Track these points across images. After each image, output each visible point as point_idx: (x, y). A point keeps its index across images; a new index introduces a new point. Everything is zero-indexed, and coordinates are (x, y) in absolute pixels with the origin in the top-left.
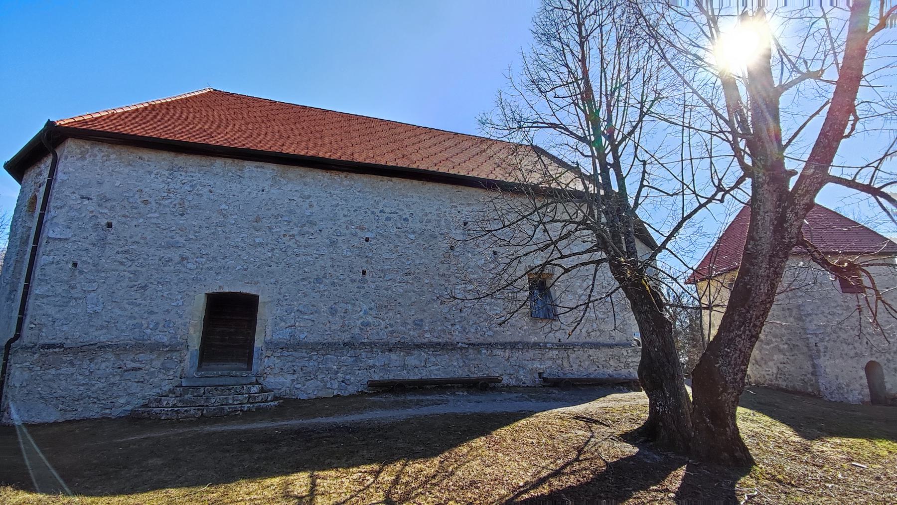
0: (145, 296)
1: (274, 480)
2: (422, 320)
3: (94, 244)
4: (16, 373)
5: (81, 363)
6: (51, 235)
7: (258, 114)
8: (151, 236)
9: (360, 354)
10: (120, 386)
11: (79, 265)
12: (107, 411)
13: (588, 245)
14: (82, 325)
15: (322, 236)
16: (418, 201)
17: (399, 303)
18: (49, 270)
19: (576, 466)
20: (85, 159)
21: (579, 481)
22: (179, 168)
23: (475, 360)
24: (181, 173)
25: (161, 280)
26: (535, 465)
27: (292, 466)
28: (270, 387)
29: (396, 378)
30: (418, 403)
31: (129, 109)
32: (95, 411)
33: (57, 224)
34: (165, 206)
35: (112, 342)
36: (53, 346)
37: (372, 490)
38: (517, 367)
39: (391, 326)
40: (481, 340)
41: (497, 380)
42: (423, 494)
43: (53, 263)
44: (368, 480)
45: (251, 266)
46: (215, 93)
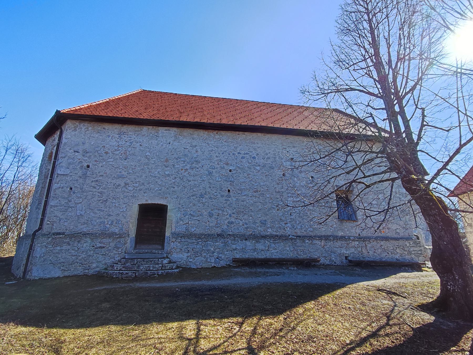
0: (106, 206)
1: (174, 324)
2: (265, 221)
3: (80, 177)
4: (38, 250)
5: (73, 243)
6: (59, 172)
7: (167, 101)
8: (109, 172)
9: (228, 242)
10: (93, 257)
11: (73, 189)
12: (87, 271)
13: (383, 169)
14: (74, 222)
15: (203, 169)
16: (261, 146)
17: (251, 210)
18: (58, 192)
19: (388, 330)
20: (76, 130)
21: (393, 342)
22: (124, 133)
23: (301, 246)
24: (125, 135)
25: (114, 197)
26: (355, 326)
27: (185, 315)
28: (174, 260)
29: (250, 257)
30: (264, 274)
31: (99, 103)
32: (80, 271)
33: (62, 167)
34: (116, 154)
35: (89, 232)
36: (59, 234)
37: (238, 337)
38: (330, 252)
39: (246, 224)
40: (305, 234)
41: (316, 260)
42: (274, 344)
43: (60, 188)
44: (235, 329)
45: (163, 188)
46: (144, 93)
